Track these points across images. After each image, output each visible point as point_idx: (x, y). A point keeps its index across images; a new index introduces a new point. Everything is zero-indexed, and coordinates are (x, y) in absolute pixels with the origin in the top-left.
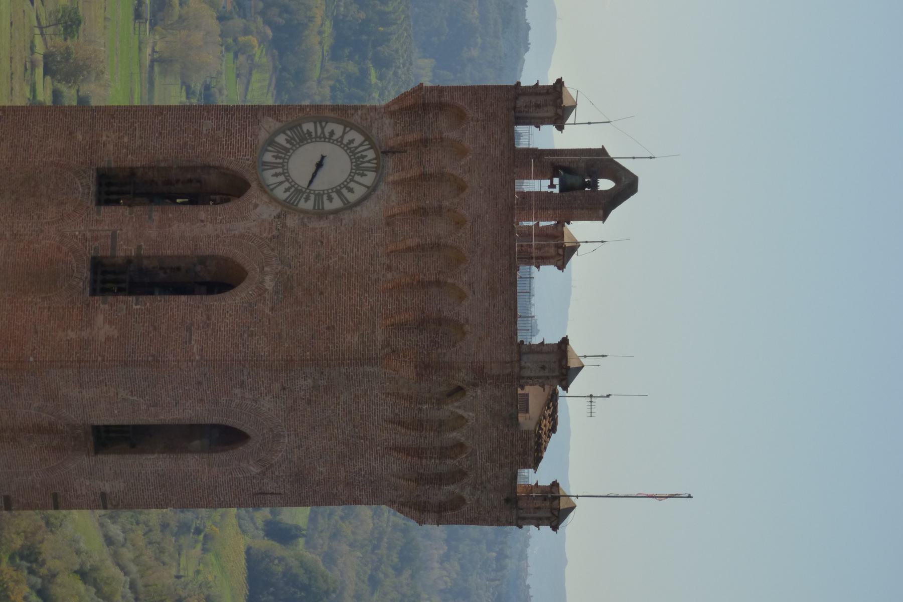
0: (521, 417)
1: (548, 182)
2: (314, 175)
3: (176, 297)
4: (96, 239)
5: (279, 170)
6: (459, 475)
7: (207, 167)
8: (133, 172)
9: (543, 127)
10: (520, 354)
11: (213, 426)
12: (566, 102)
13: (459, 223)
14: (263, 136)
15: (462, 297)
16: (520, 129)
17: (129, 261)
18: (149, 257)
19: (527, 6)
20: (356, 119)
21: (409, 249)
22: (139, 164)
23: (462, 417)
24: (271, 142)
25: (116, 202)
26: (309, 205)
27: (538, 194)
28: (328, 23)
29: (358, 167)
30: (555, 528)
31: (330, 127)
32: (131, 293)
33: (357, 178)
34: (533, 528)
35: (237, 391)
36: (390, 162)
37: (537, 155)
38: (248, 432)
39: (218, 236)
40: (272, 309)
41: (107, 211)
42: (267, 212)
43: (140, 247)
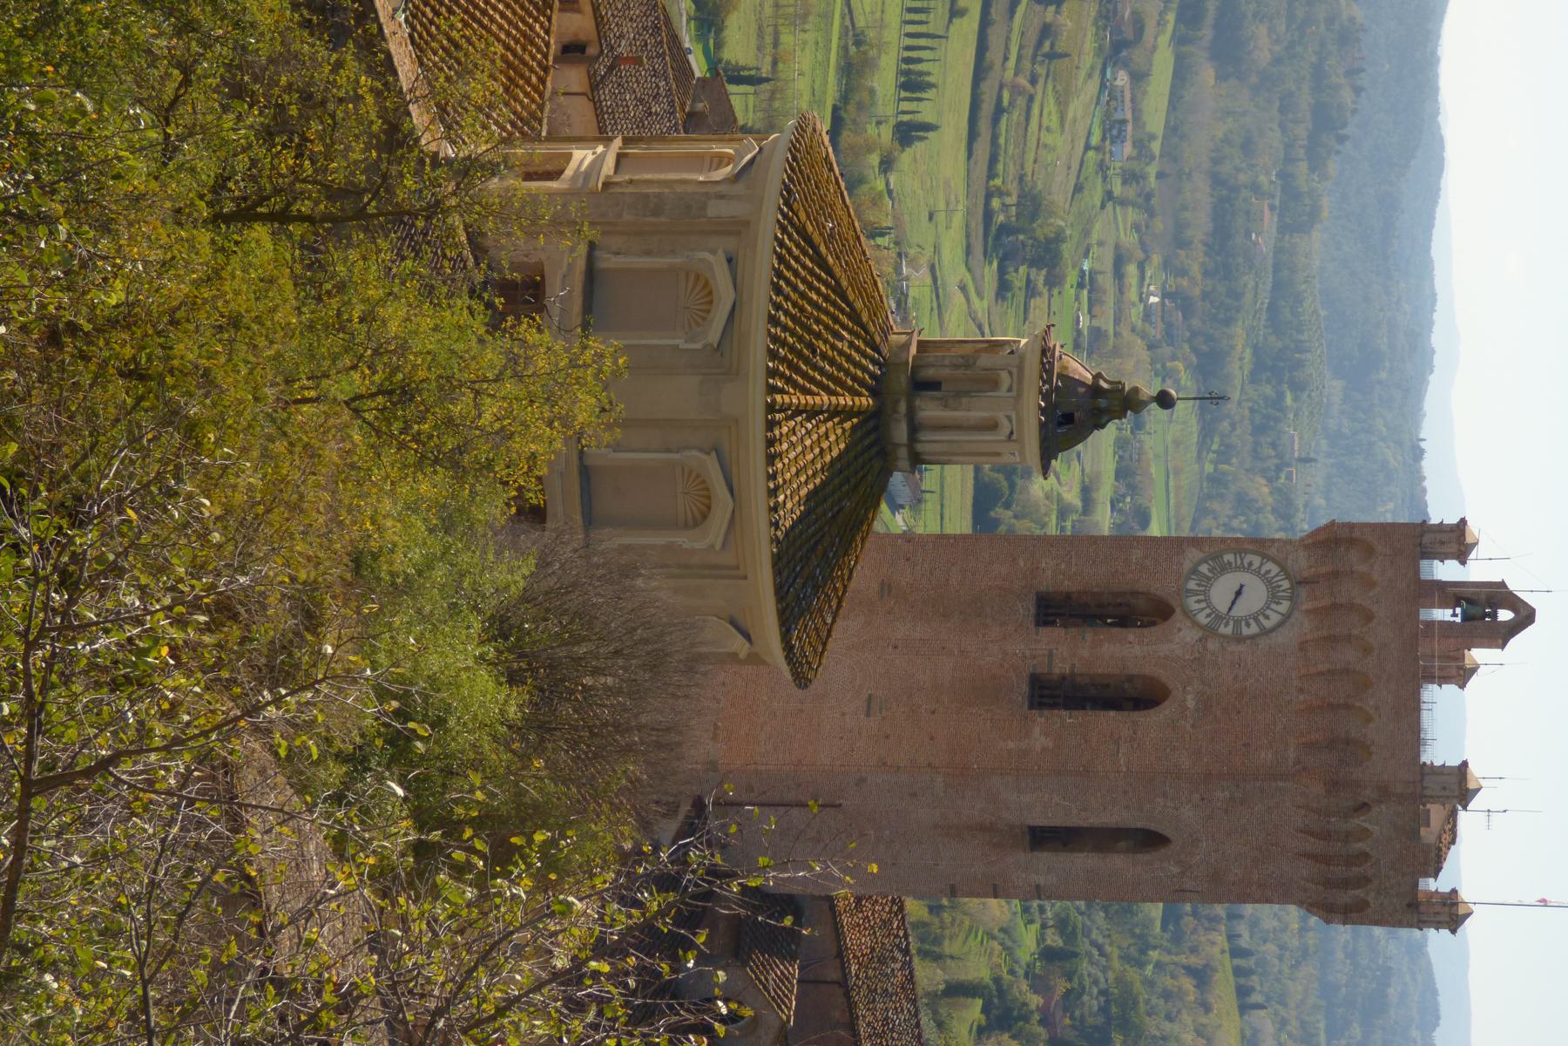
0: (1423, 831)
1: (1451, 611)
2: (1233, 603)
3: (1105, 713)
4: (1035, 657)
5: (1202, 597)
6: (1363, 881)
7: (1135, 593)
8: (1068, 596)
9: (1446, 562)
10: (1423, 775)
11: (1137, 829)
12: (1469, 540)
13: (1367, 650)
14: (1187, 565)
15: (1369, 719)
16: (1424, 563)
17: (1063, 677)
18: (1082, 675)
19: (1450, 913)
20: (1273, 551)
21: (1321, 674)
22: (1074, 589)
23: (1368, 830)
24: (1194, 571)
25: (1053, 623)
26: (1226, 630)
27: (1442, 623)
28: (1248, 351)
29: (1274, 596)
30: (1454, 931)
31: (1248, 558)
32: (1067, 707)
33: (1273, 606)
34: (1432, 931)
35: (1160, 800)
36: (1303, 592)
37: (1442, 586)
38: (1169, 836)
39: (1144, 657)
40: (1193, 726)
41: (1045, 632)
42: (1189, 635)
43: (1073, 666)
